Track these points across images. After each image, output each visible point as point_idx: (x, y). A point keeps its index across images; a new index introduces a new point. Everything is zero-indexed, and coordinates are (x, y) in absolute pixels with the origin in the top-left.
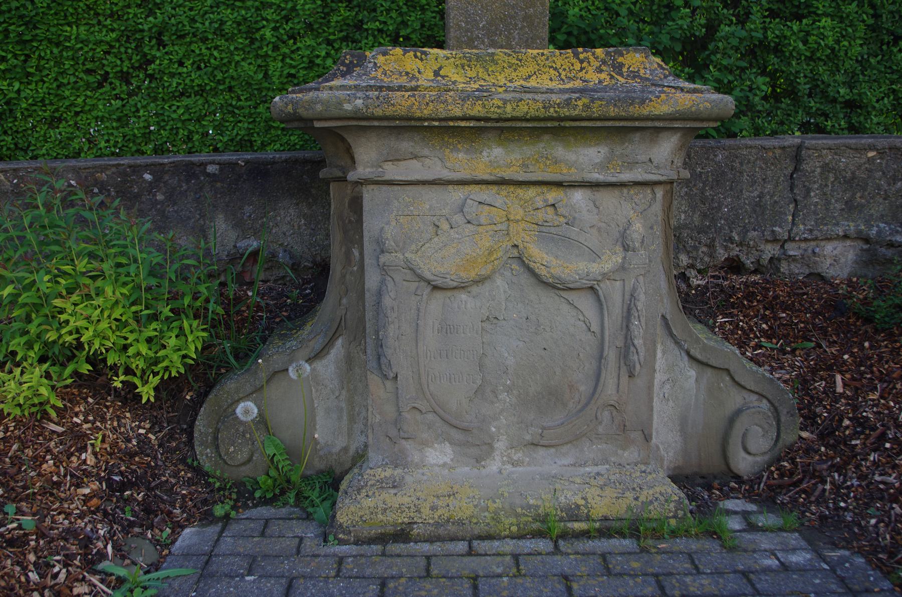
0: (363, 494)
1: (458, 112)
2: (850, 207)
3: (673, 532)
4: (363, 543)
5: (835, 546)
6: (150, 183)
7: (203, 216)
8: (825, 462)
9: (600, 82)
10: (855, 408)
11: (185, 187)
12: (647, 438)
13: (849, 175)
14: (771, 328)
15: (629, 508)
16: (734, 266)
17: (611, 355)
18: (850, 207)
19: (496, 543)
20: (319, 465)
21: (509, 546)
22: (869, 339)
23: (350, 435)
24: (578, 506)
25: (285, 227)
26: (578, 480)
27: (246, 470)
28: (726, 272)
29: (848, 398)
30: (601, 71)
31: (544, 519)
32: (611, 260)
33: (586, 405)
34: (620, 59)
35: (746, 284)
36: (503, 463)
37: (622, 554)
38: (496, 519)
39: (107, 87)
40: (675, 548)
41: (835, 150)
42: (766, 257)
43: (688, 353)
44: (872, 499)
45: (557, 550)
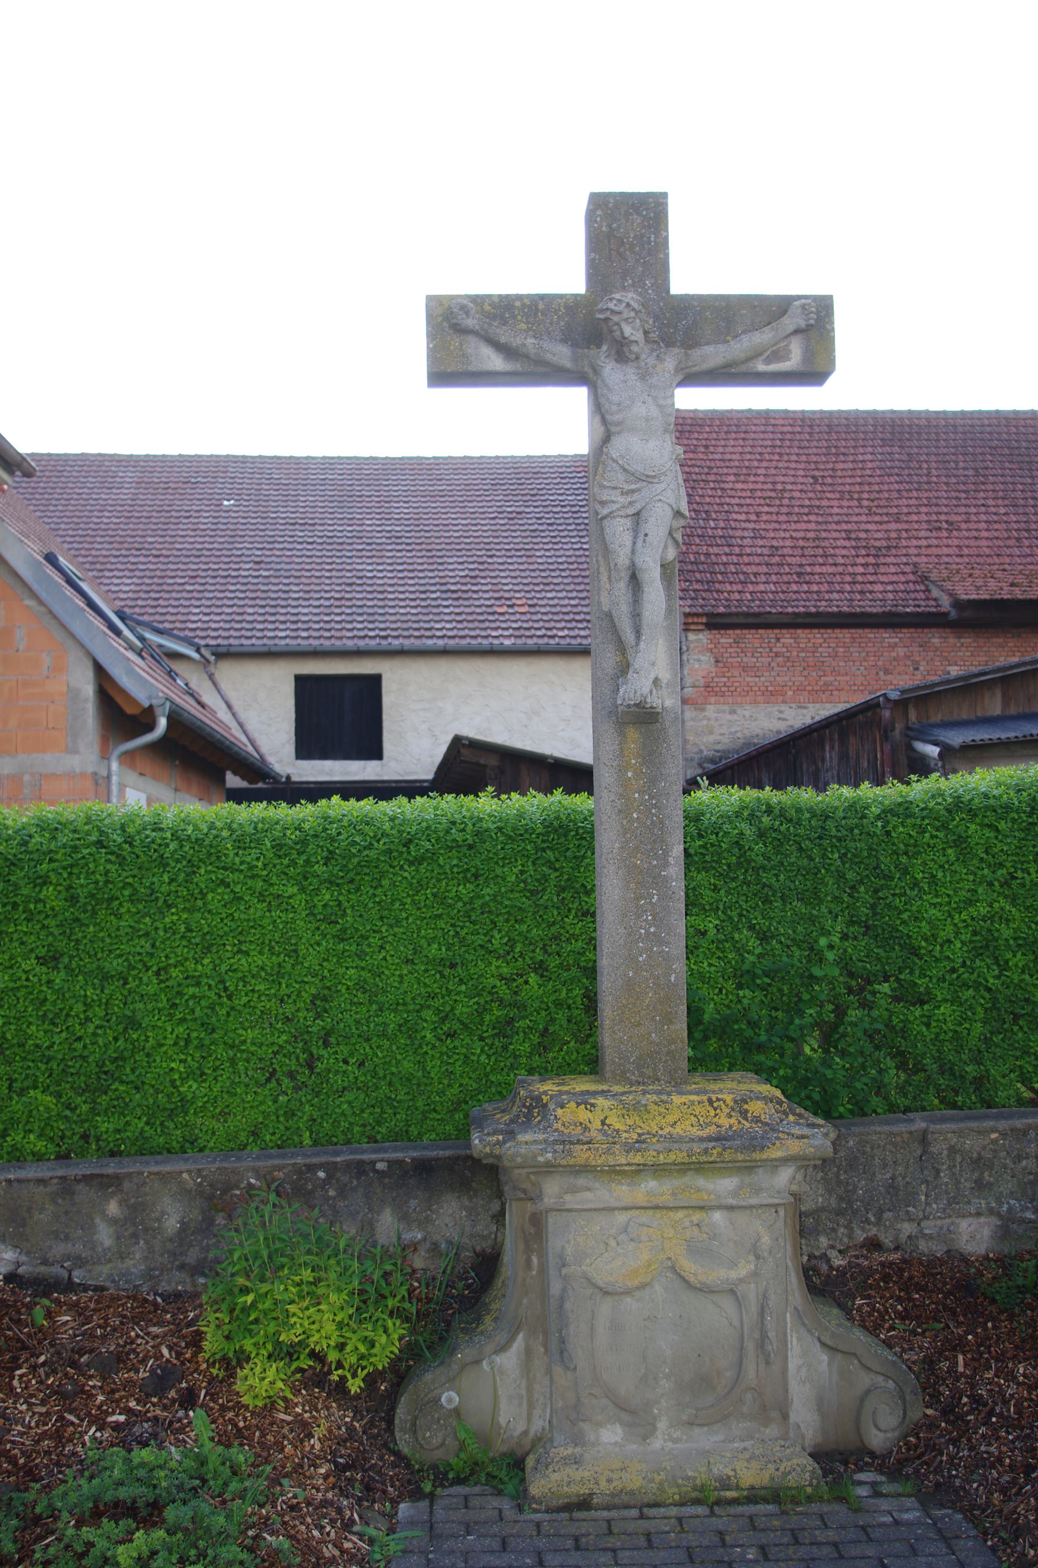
0: (551, 1469)
1: (623, 1161)
2: (980, 1186)
3: (808, 1497)
4: (553, 1511)
5: (942, 1506)
6: (324, 1180)
7: (370, 1210)
8: (943, 1436)
9: (731, 1127)
10: (973, 1386)
11: (355, 1182)
12: (785, 1417)
13: (975, 1155)
14: (905, 1309)
15: (772, 1479)
16: (873, 1245)
17: (750, 1346)
18: (980, 1186)
19: (662, 1510)
20: (504, 1448)
21: (674, 1511)
22: (993, 1319)
23: (529, 1419)
24: (729, 1477)
25: (452, 1219)
26: (728, 1455)
27: (439, 1454)
28: (868, 1250)
29: (967, 1377)
30: (731, 1117)
31: (702, 1489)
32: (744, 1269)
33: (732, 1389)
34: (746, 1106)
35: (882, 1264)
36: (665, 1441)
37: (765, 1516)
38: (661, 1489)
39: (273, 1084)
40: (810, 1511)
41: (960, 1134)
42: (903, 1237)
43: (819, 1340)
44: (977, 1467)
45: (712, 1513)
